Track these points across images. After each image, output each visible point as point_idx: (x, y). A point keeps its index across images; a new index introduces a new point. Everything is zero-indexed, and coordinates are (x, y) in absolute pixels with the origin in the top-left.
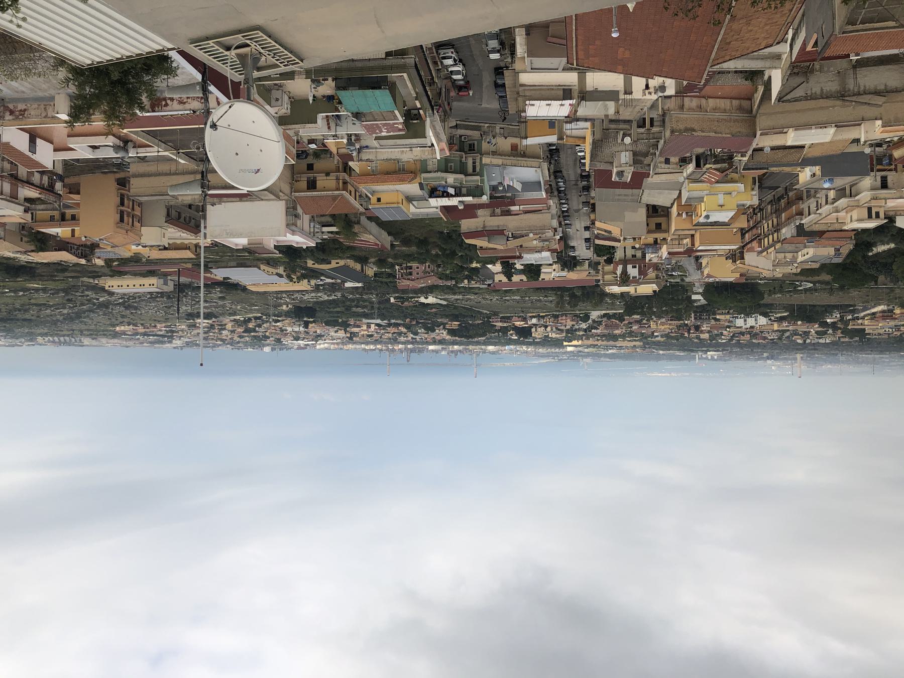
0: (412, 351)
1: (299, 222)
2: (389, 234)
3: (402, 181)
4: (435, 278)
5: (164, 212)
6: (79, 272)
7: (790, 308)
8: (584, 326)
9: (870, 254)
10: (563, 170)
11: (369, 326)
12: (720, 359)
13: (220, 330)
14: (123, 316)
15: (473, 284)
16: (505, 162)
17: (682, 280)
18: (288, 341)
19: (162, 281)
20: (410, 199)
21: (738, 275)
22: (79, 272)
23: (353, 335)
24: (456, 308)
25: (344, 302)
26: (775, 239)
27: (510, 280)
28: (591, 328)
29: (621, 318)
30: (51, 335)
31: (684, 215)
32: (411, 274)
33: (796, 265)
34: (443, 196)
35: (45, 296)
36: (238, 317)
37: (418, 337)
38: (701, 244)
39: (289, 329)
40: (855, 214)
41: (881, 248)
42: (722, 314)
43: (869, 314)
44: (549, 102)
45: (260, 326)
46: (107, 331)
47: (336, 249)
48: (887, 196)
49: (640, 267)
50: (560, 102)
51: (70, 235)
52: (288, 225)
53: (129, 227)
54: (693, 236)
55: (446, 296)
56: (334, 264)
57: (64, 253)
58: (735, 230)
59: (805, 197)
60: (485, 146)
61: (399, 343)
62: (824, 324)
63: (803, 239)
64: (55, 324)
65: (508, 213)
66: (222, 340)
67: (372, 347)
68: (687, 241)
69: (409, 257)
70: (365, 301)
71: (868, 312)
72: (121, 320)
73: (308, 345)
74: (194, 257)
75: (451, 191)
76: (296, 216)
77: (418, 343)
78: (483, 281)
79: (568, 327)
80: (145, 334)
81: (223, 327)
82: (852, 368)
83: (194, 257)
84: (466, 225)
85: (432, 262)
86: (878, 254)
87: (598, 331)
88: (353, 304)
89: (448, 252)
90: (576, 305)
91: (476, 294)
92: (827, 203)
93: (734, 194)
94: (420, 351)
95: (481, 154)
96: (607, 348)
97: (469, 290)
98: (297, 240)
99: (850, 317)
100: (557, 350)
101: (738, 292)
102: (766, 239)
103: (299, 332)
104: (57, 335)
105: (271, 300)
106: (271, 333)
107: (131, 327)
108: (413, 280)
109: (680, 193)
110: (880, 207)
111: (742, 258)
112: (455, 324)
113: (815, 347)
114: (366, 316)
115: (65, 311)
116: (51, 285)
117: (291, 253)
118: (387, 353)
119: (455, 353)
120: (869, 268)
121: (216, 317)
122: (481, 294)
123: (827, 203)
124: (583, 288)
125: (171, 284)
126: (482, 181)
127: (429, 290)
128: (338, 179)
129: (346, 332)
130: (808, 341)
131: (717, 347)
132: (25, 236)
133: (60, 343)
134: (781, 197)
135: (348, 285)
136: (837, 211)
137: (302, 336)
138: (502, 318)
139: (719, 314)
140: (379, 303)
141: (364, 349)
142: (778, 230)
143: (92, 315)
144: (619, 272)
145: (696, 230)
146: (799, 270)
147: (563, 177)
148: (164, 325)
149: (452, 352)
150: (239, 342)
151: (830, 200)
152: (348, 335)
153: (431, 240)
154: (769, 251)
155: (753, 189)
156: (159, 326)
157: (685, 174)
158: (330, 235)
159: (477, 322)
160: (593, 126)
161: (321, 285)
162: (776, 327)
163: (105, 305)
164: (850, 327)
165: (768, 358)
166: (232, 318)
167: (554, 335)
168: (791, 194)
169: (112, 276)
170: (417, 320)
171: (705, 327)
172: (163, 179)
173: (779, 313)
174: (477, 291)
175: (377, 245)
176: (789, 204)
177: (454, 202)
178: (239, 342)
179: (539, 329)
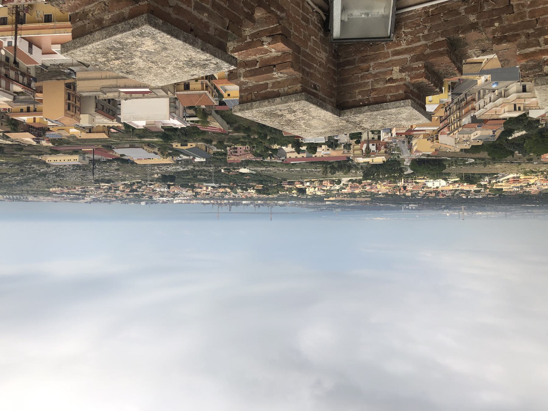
0: (232, 204)
1: (177, 112)
4: (251, 155)
5: (94, 105)
6: (30, 151)
7: (459, 175)
9: (510, 138)
12: (416, 209)
13: (117, 190)
14: (55, 182)
17: (398, 157)
21: (434, 150)
22: (30, 151)
23: (197, 194)
24: (261, 176)
25: (193, 172)
28: (342, 188)
29: (360, 182)
30: (8, 194)
32: (236, 152)
33: (468, 143)
35: (6, 167)
36: (126, 182)
37: (237, 196)
39: (158, 190)
40: (506, 108)
41: (517, 134)
42: (420, 179)
45: (140, 187)
46: (44, 191)
47: (195, 133)
48: (526, 96)
49: (376, 146)
51: (33, 121)
52: (170, 113)
55: (256, 169)
56: (189, 146)
58: (437, 118)
59: (477, 99)
63: (476, 125)
64: (11, 187)
66: (116, 197)
67: (208, 202)
69: (236, 141)
70: (206, 171)
72: (53, 184)
77: (236, 199)
79: (328, 188)
80: (68, 193)
81: (117, 189)
85: (251, 144)
86: (515, 138)
88: (199, 173)
89: (263, 135)
90: (335, 173)
91: (274, 167)
92: (490, 101)
94: (237, 204)
96: (349, 202)
97: (270, 164)
98: (176, 123)
99: (494, 181)
100: (320, 204)
101: (431, 164)
102: (453, 126)
103: (164, 192)
104: (13, 194)
105: (149, 171)
106: (146, 193)
107: (60, 188)
108: (237, 156)
110: (521, 104)
111: (437, 139)
112: (260, 187)
115: (18, 178)
116: (11, 160)
117: (169, 133)
118: (217, 206)
119: (259, 205)
120: (509, 147)
121: (113, 182)
123: (490, 101)
124: (339, 162)
125: (87, 159)
127: (245, 164)
128: (202, 84)
133: (13, 199)
134: (463, 100)
135: (197, 160)
136: (496, 107)
139: (418, 179)
141: (203, 203)
142: (460, 120)
144: (364, 149)
146: (470, 146)
148: (80, 187)
149: (257, 205)
150: (126, 199)
151: (492, 99)
152: (194, 194)
153: (252, 128)
154: (454, 133)
155: (449, 92)
156: (77, 188)
158: (192, 123)
159: (274, 185)
161: (180, 161)
163: (44, 174)
164: (494, 187)
165: (445, 208)
166: (123, 182)
169: (50, 154)
172: (97, 82)
174: (274, 165)
175: (220, 129)
176: (467, 104)
178: (126, 199)
179: (310, 189)
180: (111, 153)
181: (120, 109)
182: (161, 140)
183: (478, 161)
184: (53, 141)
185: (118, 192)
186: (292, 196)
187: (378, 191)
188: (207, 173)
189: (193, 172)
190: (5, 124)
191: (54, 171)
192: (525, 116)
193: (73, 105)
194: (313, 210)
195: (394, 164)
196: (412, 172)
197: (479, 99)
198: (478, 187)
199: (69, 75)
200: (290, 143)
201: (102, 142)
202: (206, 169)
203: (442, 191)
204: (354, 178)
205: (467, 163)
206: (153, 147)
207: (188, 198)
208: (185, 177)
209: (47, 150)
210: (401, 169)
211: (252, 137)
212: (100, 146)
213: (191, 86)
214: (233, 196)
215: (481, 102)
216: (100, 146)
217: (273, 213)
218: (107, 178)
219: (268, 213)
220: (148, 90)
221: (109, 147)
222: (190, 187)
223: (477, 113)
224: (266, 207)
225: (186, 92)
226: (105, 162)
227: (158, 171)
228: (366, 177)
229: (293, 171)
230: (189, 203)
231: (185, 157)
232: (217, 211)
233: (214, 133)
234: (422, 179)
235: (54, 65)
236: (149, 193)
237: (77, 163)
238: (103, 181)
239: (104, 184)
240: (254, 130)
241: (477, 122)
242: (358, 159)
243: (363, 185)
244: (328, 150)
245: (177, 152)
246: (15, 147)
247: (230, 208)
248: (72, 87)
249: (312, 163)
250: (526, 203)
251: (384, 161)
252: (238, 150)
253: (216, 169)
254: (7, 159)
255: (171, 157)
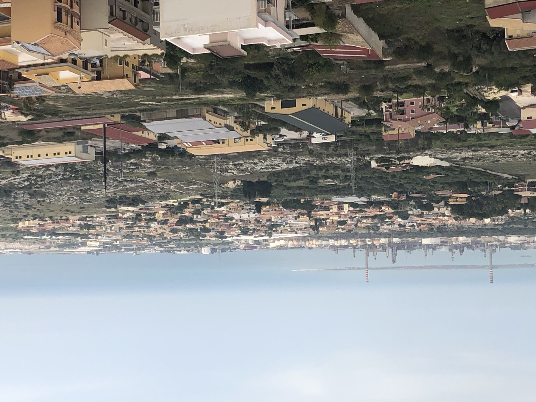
0: (399, 247)
1: (273, 9)
2: (381, 37)
5: (106, 9)
11: (341, 208)
13: (149, 221)
14: (28, 207)
15: (490, 128)
19: (80, 147)
25: (308, 172)
32: (403, 112)
36: (170, 202)
39: (236, 216)
45: (198, 212)
46: (7, 229)
47: (310, 66)
52: (259, 13)
53: (69, 29)
61: (381, 235)
67: (343, 242)
70: (336, 168)
72: (25, 212)
73: (258, 242)
74: (133, 87)
77: (409, 234)
78: (504, 121)
80: (53, 233)
83: (133, 87)
85: (435, 89)
88: (323, 172)
89: (461, 58)
91: (492, 147)
94: (410, 247)
106: (212, 224)
107: (37, 221)
112: (461, 198)
118: (364, 251)
119: (461, 248)
121: (143, 202)
122: (499, 147)
125: (92, 152)
127: (425, 141)
129: (310, 216)
135: (318, 138)
137: (252, 226)
140: (357, 169)
141: (333, 247)
148: (78, 217)
149: (456, 247)
152: (313, 223)
156: (71, 218)
158: (304, 43)
166: (164, 203)
169: (20, 143)
170: (410, 191)
174: (493, 142)
175: (365, 51)
180: (139, 133)
181: (158, 13)
185: (154, 225)
191: (26, 183)
193: (67, 12)
200: (526, 80)
202: (337, 161)
206: (224, 115)
207: (300, 234)
208: (293, 184)
209: (14, 135)
211: (437, 70)
212: (117, 118)
214: (400, 226)
216: (117, 118)
217: (497, 267)
218: (131, 193)
219: (483, 267)
221: (134, 121)
222: (302, 206)
224: (478, 251)
226: (127, 156)
227: (235, 172)
230: (302, 247)
231: (291, 135)
232: (364, 271)
233: (350, 62)
236: (217, 224)
238: (124, 201)
239: (125, 208)
240: (440, 53)
245: (273, 124)
252: (408, 109)
255: (261, 136)
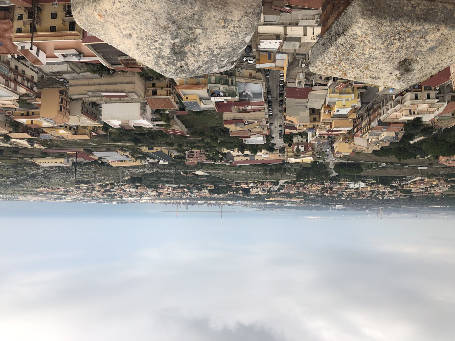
0: (189, 204)
1: (146, 114)
2: (186, 127)
3: (199, 88)
5: (80, 108)
6: (25, 154)
7: (374, 178)
8: (276, 188)
9: (411, 142)
10: (271, 92)
11: (168, 189)
12: (342, 209)
13: (92, 190)
15: (223, 163)
16: (246, 81)
17: (324, 161)
18: (126, 198)
19: (66, 160)
20: (201, 99)
23: (160, 194)
24: (213, 177)
25: (157, 174)
26: (369, 128)
27: (243, 154)
28: (279, 189)
29: (294, 183)
31: (327, 112)
33: (378, 144)
34: (217, 96)
35: (3, 170)
36: (102, 183)
38: (335, 126)
39: (128, 190)
40: (404, 113)
42: (343, 181)
43: (413, 182)
44: (270, 41)
45: (113, 188)
46: (33, 191)
47: (160, 135)
48: (418, 103)
50: (275, 41)
51: (30, 123)
52: (141, 114)
54: (331, 123)
57: (26, 134)
58: (350, 120)
60: (237, 73)
62: (392, 187)
65: (245, 111)
66: (93, 197)
67: (169, 201)
68: (328, 126)
69: (193, 145)
70: (168, 174)
71: (412, 180)
72: (41, 185)
73: (136, 200)
75: (221, 94)
76: (145, 111)
77: (193, 199)
78: (228, 160)
80: (52, 193)
82: (406, 215)
84: (227, 116)
87: (283, 191)
88: (163, 175)
89: (214, 138)
90: (273, 174)
91: (224, 169)
92: (391, 108)
93: (350, 100)
94: (193, 204)
95: (236, 77)
96: (286, 202)
98: (146, 123)
99: (404, 183)
100: (262, 204)
103: (132, 192)
105: (121, 174)
106: (118, 193)
107: (46, 189)
109: (325, 101)
110: (415, 109)
112: (212, 187)
113: (389, 201)
114: (168, 182)
115: (12, 179)
116: (8, 163)
118: (176, 205)
119: (211, 205)
121: (91, 183)
122: (226, 169)
126: (236, 89)
127: (200, 166)
129: (157, 191)
130: (385, 198)
131: (341, 202)
132: (7, 123)
133: (6, 199)
135: (161, 162)
136: (396, 111)
137: (134, 194)
138: (236, 183)
140: (175, 175)
141: (165, 203)
142: (370, 124)
143: (26, 182)
144: (295, 150)
145: (332, 120)
147: (271, 95)
148: (63, 188)
149: (209, 204)
152: (158, 194)
154: (366, 134)
156: (60, 188)
157: (328, 86)
158: (158, 127)
160: (289, 56)
162: (369, 188)
163: (34, 176)
164: (404, 188)
165: (365, 209)
166: (99, 184)
167: (261, 193)
168: (375, 106)
169: (41, 157)
171: (335, 189)
172: (84, 87)
173: (369, 181)
174: (224, 168)
175: (180, 132)
176: (375, 111)
177: (222, 99)
179: (254, 190)
180: (91, 156)
181: (101, 111)
182: (133, 144)
183: (389, 166)
184: (44, 143)
185: (94, 192)
186: (239, 197)
187: (309, 192)
188: (168, 175)
189: (157, 174)
190: (9, 125)
191: (42, 173)
192: (418, 120)
193: (64, 108)
194: (256, 209)
195: (322, 167)
196: (337, 174)
197: (383, 106)
198: (392, 189)
199: (62, 84)
200: (236, 147)
201: (84, 145)
203: (362, 192)
204: (289, 180)
205: (380, 167)
206: (125, 151)
208: (151, 179)
210: (327, 172)
211: (206, 141)
212: (82, 150)
213: (158, 93)
215: (384, 109)
216: (82, 150)
217: (223, 212)
219: (219, 212)
220: (124, 94)
221: (90, 151)
222: (154, 187)
223: (382, 118)
224: (217, 206)
225: (153, 97)
226: (85, 165)
228: (299, 177)
229: (239, 173)
230: (153, 203)
231: (152, 160)
233: (174, 135)
234: (345, 181)
235: (53, 72)
236: (120, 193)
237: (62, 165)
238: (83, 182)
239: (83, 185)
241: (384, 125)
242: (291, 159)
243: (297, 186)
244: (267, 153)
245: (144, 156)
246: (12, 149)
247: (187, 207)
248: (64, 93)
249: (255, 165)
250: (432, 204)
251: (312, 162)
252: (195, 154)
253: (176, 171)
254: (5, 161)
